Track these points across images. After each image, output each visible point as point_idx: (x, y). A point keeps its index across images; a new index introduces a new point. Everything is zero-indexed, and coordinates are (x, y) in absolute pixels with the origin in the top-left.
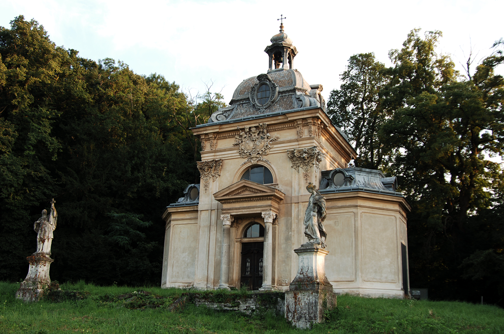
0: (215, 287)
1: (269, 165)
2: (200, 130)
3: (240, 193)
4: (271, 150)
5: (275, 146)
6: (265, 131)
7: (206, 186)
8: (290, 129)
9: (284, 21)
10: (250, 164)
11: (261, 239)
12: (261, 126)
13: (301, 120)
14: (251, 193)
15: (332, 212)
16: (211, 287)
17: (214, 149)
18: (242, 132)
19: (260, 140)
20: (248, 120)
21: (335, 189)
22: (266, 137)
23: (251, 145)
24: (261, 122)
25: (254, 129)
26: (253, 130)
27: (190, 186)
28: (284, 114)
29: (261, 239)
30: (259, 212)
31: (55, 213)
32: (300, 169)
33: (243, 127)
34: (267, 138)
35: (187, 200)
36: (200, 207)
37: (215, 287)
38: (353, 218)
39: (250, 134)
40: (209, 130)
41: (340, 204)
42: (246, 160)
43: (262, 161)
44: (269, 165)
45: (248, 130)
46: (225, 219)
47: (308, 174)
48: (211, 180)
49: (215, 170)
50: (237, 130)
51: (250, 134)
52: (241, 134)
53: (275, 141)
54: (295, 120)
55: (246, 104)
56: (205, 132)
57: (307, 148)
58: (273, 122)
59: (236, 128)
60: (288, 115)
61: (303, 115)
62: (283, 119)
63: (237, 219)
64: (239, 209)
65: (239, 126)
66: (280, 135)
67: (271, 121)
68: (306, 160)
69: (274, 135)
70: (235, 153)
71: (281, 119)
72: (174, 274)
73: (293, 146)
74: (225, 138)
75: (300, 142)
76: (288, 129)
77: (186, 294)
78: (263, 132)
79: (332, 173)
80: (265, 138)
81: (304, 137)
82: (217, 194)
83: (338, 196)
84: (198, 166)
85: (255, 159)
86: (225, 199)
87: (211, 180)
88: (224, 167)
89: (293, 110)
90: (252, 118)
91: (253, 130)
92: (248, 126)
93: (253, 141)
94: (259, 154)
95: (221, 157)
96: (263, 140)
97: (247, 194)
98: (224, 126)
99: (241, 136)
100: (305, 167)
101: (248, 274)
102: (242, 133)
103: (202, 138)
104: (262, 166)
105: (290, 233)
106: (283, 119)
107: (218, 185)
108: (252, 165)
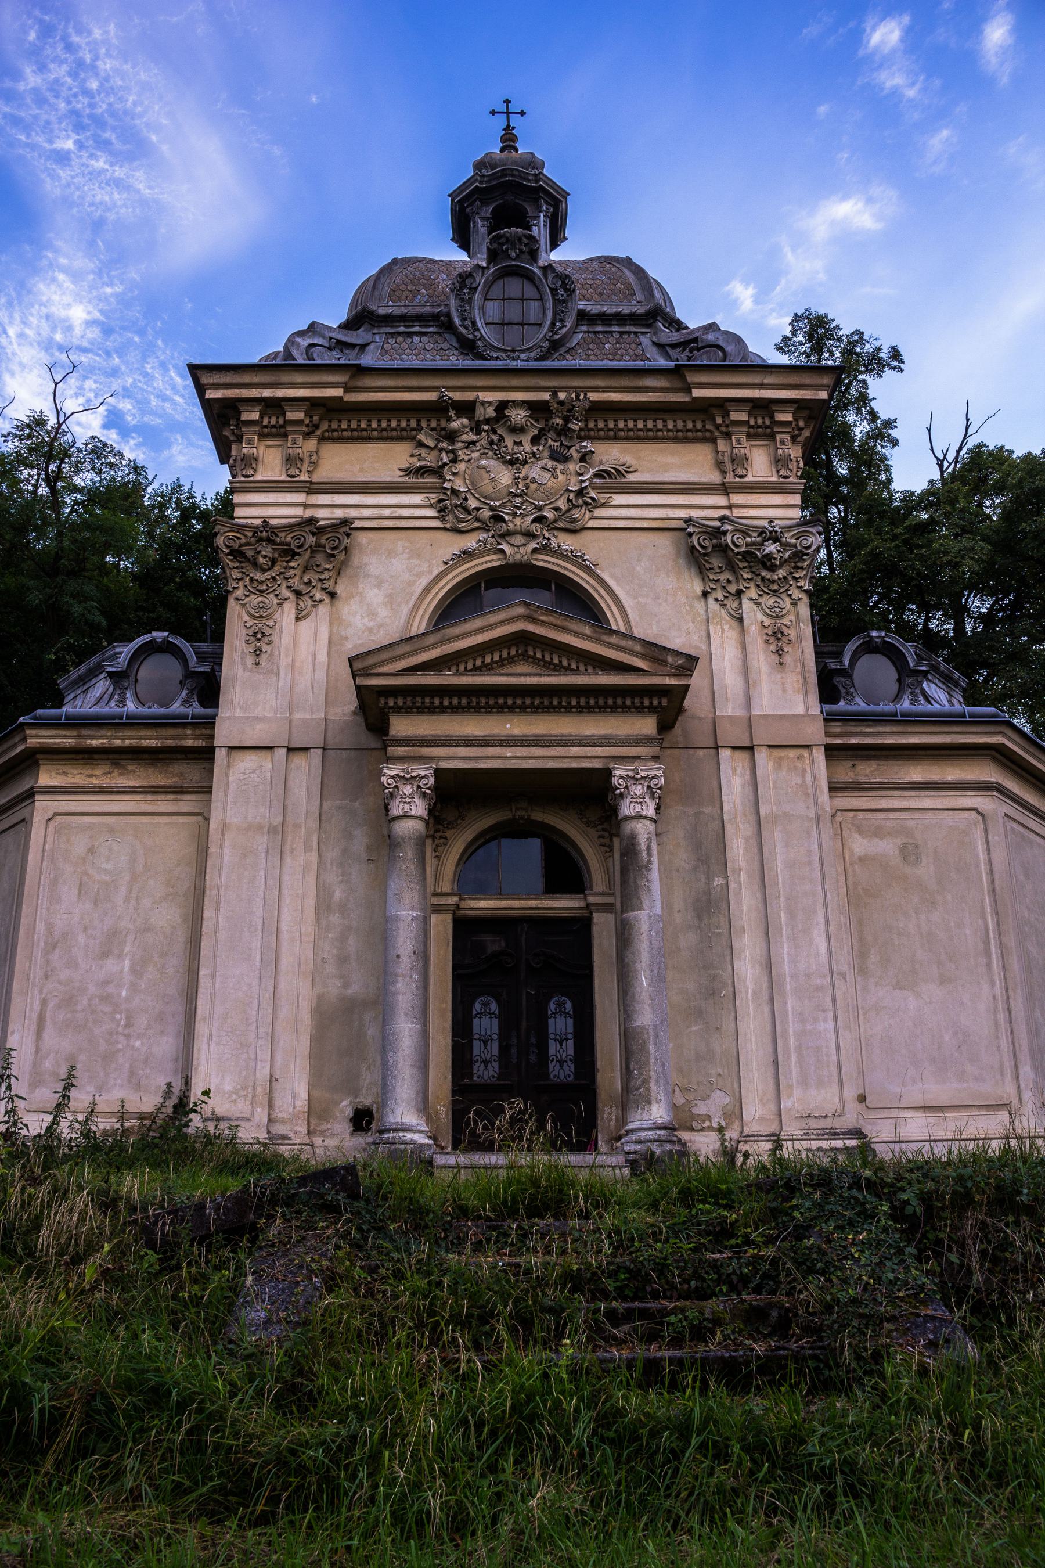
0: (318, 1141)
4: (599, 512)
5: (619, 499)
7: (259, 637)
8: (686, 440)
9: (515, 121)
10: (492, 561)
11: (564, 904)
12: (561, 403)
15: (884, 804)
16: (336, 1143)
17: (304, 477)
18: (459, 416)
19: (550, 464)
23: (505, 477)
24: (563, 388)
27: (159, 635)
29: (564, 904)
30: (597, 764)
32: (746, 604)
33: (469, 396)
34: (583, 459)
36: (224, 734)
37: (318, 1141)
38: (978, 833)
39: (495, 432)
41: (917, 773)
42: (470, 542)
44: (588, 570)
45: (491, 412)
46: (408, 790)
47: (786, 631)
49: (306, 569)
51: (495, 432)
52: (455, 425)
53: (614, 479)
55: (425, 339)
56: (267, 393)
60: (691, 378)
61: (762, 386)
63: (455, 795)
64: (485, 742)
65: (449, 388)
66: (639, 459)
67: (606, 389)
68: (773, 569)
69: (610, 454)
70: (416, 506)
72: (48, 1064)
73: (707, 508)
74: (362, 437)
75: (737, 498)
76: (676, 439)
77: (273, 1202)
80: (565, 459)
82: (370, 661)
83: (948, 734)
84: (220, 541)
86: (380, 701)
87: (288, 612)
88: (356, 560)
91: (518, 416)
93: (512, 462)
94: (540, 519)
96: (560, 467)
97: (524, 675)
99: (451, 436)
100: (769, 601)
101: (485, 1073)
103: (245, 416)
105: (718, 881)
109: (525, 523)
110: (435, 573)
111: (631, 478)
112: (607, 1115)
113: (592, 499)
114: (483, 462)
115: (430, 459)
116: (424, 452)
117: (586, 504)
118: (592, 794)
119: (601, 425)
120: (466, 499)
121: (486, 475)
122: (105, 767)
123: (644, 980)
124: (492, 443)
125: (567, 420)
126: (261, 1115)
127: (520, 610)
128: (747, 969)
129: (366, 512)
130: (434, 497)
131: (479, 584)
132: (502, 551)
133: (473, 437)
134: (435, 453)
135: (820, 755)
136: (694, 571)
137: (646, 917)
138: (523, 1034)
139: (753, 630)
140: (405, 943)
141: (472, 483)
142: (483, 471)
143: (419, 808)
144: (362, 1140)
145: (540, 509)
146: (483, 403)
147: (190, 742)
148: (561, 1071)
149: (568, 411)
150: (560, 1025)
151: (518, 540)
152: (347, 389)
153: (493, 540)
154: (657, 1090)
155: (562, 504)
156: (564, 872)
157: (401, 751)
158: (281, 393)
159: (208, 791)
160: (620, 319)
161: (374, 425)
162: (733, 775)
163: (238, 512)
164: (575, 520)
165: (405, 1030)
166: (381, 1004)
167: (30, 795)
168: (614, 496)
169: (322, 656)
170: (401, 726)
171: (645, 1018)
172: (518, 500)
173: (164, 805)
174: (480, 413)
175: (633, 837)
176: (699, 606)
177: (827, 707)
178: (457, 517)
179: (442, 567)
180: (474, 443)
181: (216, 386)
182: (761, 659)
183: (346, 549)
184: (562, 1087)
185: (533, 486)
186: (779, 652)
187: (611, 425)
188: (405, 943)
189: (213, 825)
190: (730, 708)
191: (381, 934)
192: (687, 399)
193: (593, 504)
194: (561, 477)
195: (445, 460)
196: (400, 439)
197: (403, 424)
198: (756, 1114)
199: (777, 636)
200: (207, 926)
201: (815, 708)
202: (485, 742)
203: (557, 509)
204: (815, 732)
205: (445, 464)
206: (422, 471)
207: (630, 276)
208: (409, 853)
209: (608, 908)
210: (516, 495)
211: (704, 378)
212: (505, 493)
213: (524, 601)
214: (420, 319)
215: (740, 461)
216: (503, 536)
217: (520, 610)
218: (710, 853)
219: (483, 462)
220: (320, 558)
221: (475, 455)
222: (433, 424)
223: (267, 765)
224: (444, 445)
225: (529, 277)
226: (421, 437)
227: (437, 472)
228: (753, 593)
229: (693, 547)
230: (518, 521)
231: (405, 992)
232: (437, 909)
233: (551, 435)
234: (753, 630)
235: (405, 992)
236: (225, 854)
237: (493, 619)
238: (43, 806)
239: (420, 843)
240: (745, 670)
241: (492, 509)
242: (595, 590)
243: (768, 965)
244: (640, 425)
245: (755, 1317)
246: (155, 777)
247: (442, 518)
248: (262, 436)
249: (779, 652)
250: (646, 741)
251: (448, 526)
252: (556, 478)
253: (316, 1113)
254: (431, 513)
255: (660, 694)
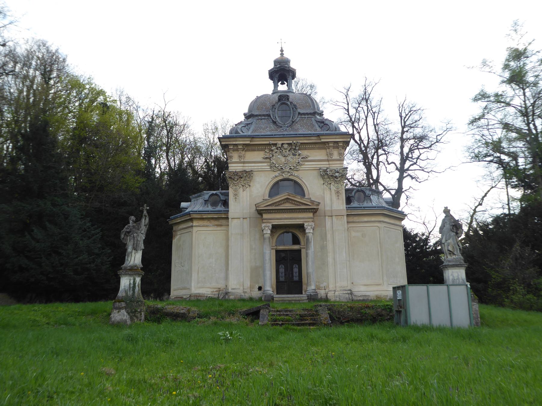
2: (230, 140)
3: (281, 204)
4: (302, 166)
5: (306, 163)
6: (297, 148)
10: (281, 178)
11: (296, 247)
14: (292, 205)
15: (359, 225)
19: (292, 156)
21: (358, 206)
23: (283, 159)
25: (287, 145)
26: (286, 146)
28: (318, 136)
29: (296, 247)
30: (302, 223)
31: (147, 219)
32: (332, 186)
35: (208, 207)
36: (230, 215)
40: (240, 141)
41: (366, 219)
42: (277, 174)
43: (294, 176)
45: (280, 146)
46: (267, 228)
48: (241, 189)
50: (269, 145)
52: (273, 148)
54: (328, 142)
56: (234, 143)
57: (339, 168)
58: (305, 141)
60: (321, 137)
63: (275, 228)
64: (281, 219)
69: (304, 153)
71: (314, 140)
73: (324, 165)
75: (331, 163)
78: (295, 149)
79: (354, 191)
80: (296, 155)
81: (333, 158)
87: (241, 189)
89: (328, 132)
91: (286, 146)
92: (280, 142)
94: (291, 169)
95: (253, 168)
97: (288, 206)
99: (272, 151)
100: (336, 185)
101: (282, 279)
104: (291, 180)
105: (325, 243)
107: (248, 194)
109: (288, 170)
111: (309, 159)
112: (304, 287)
118: (301, 227)
122: (206, 221)
123: (310, 263)
126: (242, 288)
127: (287, 194)
128: (330, 260)
129: (255, 168)
135: (345, 217)
137: (311, 251)
138: (289, 271)
139: (333, 191)
140: (267, 257)
143: (269, 232)
144: (260, 292)
147: (223, 216)
148: (296, 279)
150: (296, 270)
151: (286, 173)
152: (251, 141)
154: (313, 283)
155: (295, 165)
156: (296, 241)
157: (265, 221)
158: (237, 143)
159: (228, 225)
160: (307, 114)
162: (328, 221)
163: (230, 168)
165: (268, 273)
166: (263, 267)
167: (192, 226)
169: (248, 199)
170: (265, 216)
171: (310, 270)
173: (219, 228)
174: (278, 146)
175: (308, 237)
176: (322, 186)
177: (348, 206)
181: (223, 141)
182: (334, 197)
184: (296, 282)
186: (338, 196)
188: (267, 257)
189: (230, 234)
190: (328, 208)
191: (263, 255)
198: (331, 287)
199: (338, 192)
200: (230, 253)
201: (345, 206)
202: (281, 219)
204: (345, 213)
206: (266, 158)
207: (310, 101)
208: (267, 241)
209: (304, 248)
211: (324, 137)
213: (287, 187)
214: (264, 115)
215: (331, 154)
217: (287, 194)
218: (324, 237)
220: (247, 178)
223: (239, 222)
225: (287, 105)
228: (333, 183)
231: (268, 266)
232: (272, 249)
234: (333, 191)
235: (268, 266)
236: (232, 240)
237: (282, 196)
238: (195, 229)
239: (269, 238)
240: (331, 200)
243: (334, 259)
245: (312, 319)
246: (216, 223)
248: (233, 151)
249: (338, 196)
250: (311, 218)
253: (251, 287)
254: (269, 167)
255: (314, 210)
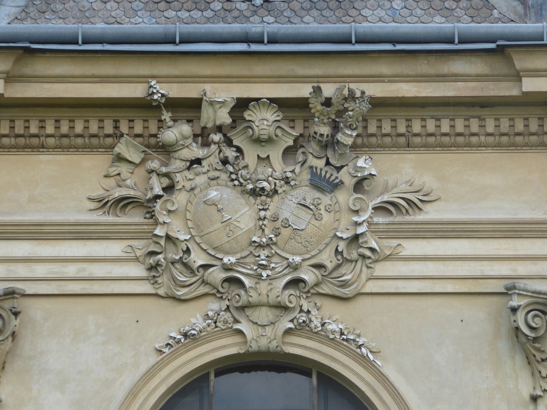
1: (364, 360)
4: (381, 269)
5: (412, 247)
8: (513, 146)
10: (226, 348)
12: (328, 103)
13: (21, 51)
20: (253, 50)
22: (349, 182)
23: (243, 215)
26: (263, 120)
28: (501, 49)
34: (359, 186)
39: (229, 142)
42: (194, 317)
43: (322, 335)
44: (364, 360)
45: (224, 117)
50: (146, 106)
51: (229, 142)
59: (135, 91)
60: (522, 62)
62: (478, 78)
69: (397, 171)
71: (466, 80)
76: (498, 146)
78: (330, 144)
80: (335, 186)
85: (263, 315)
88: (27, 345)
90: (247, 39)
91: (263, 120)
92: (227, 93)
93: (255, 193)
94: (296, 283)
96: (326, 199)
98: (40, 67)
99: (166, 150)
102: (176, 132)
104: (300, 367)
106: (478, 78)
108: (247, 354)
110: (144, 367)
111: (431, 213)
113: (372, 250)
114: (213, 194)
115: (133, 184)
116: (124, 169)
117: (363, 257)
119: (387, 128)
120: (188, 251)
121: (216, 216)
124: (225, 162)
125: (336, 127)
129: (40, 270)
130: (141, 246)
131: (208, 374)
132: (240, 332)
133: (197, 152)
134: (141, 172)
136: (520, 360)
141: (197, 226)
142: (213, 209)
145: (296, 268)
146: (212, 103)
149: (337, 112)
151: (263, 315)
153: (226, 316)
155: (328, 259)
161: (50, 129)
164: (344, 284)
168: (405, 243)
172: (263, 254)
174: (210, 116)
178: (174, 279)
179: (154, 359)
180: (198, 161)
183: (13, 334)
185: (286, 233)
187: (402, 129)
192: (515, 92)
193: (375, 256)
194: (327, 217)
195: (158, 190)
196: (88, 148)
197: (94, 128)
203: (319, 266)
205: (158, 197)
206: (124, 203)
210: (260, 246)
212: (244, 242)
216: (242, 308)
219: (213, 194)
221: (201, 180)
222: (138, 129)
224: (154, 164)
226: (122, 148)
227: (147, 206)
229: (517, 328)
230: (263, 287)
233: (313, 147)
241: (227, 268)
242: (375, 392)
244: (445, 127)
247: (153, 281)
251: (161, 292)
252: (317, 218)
